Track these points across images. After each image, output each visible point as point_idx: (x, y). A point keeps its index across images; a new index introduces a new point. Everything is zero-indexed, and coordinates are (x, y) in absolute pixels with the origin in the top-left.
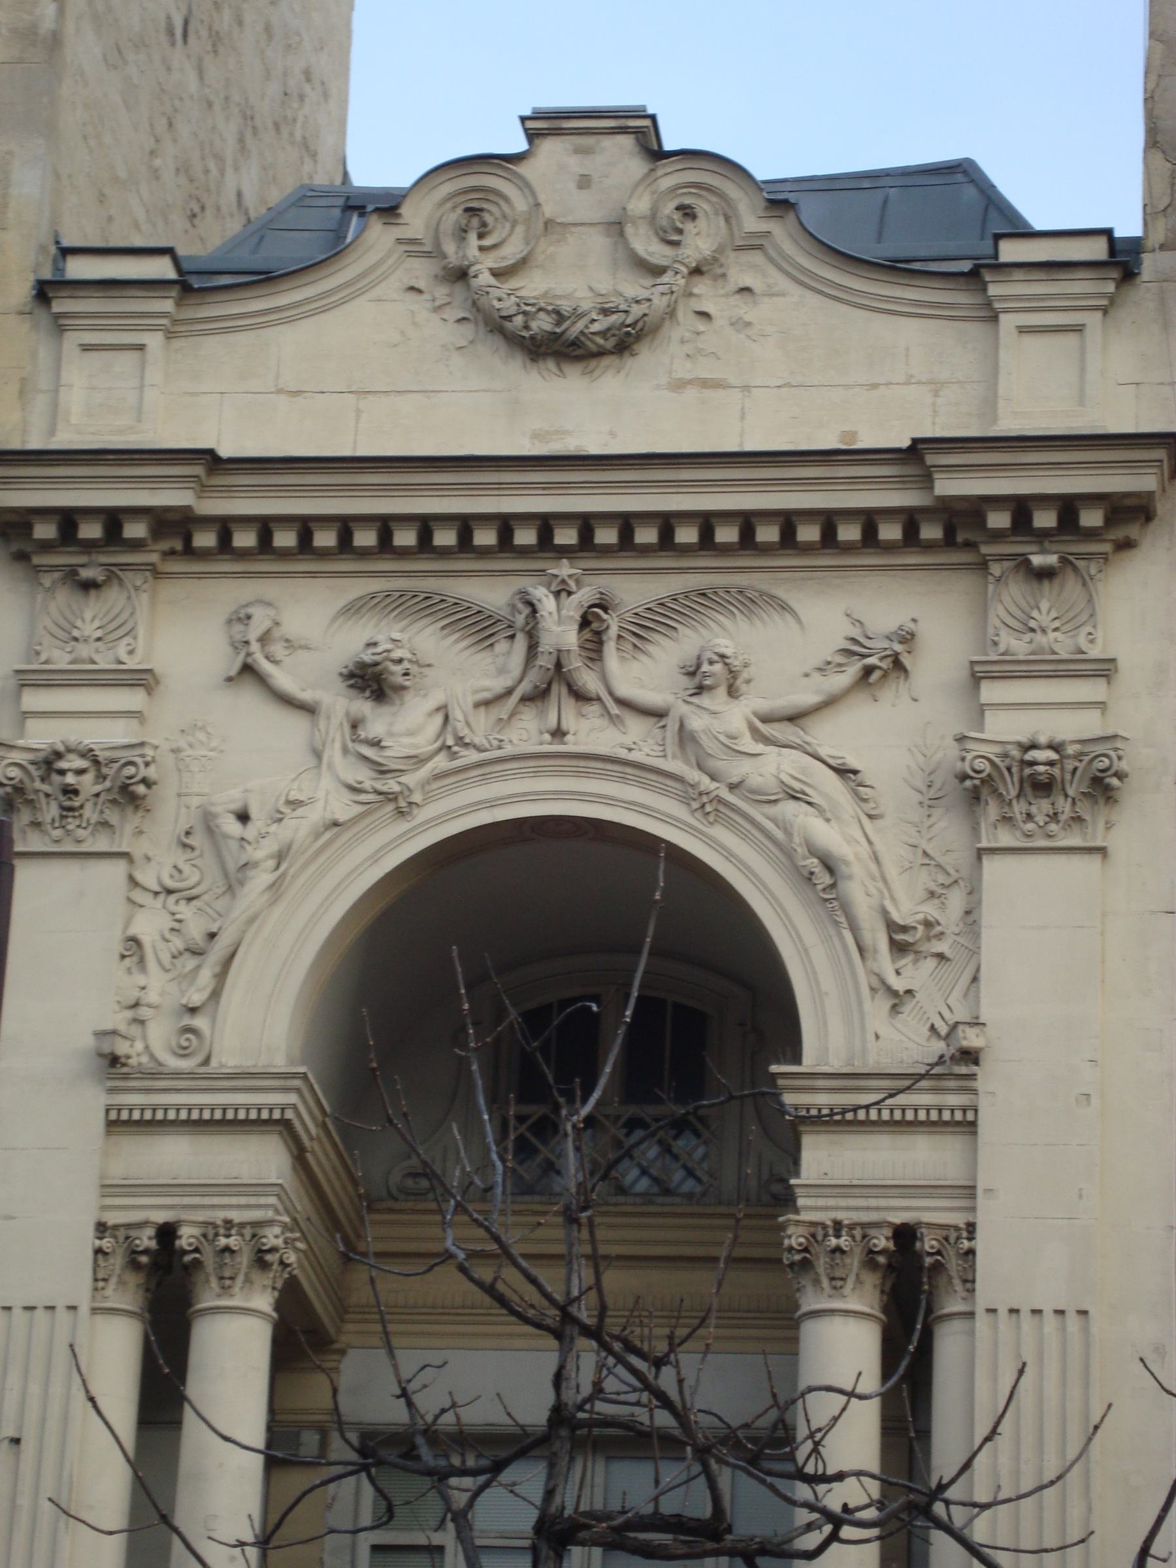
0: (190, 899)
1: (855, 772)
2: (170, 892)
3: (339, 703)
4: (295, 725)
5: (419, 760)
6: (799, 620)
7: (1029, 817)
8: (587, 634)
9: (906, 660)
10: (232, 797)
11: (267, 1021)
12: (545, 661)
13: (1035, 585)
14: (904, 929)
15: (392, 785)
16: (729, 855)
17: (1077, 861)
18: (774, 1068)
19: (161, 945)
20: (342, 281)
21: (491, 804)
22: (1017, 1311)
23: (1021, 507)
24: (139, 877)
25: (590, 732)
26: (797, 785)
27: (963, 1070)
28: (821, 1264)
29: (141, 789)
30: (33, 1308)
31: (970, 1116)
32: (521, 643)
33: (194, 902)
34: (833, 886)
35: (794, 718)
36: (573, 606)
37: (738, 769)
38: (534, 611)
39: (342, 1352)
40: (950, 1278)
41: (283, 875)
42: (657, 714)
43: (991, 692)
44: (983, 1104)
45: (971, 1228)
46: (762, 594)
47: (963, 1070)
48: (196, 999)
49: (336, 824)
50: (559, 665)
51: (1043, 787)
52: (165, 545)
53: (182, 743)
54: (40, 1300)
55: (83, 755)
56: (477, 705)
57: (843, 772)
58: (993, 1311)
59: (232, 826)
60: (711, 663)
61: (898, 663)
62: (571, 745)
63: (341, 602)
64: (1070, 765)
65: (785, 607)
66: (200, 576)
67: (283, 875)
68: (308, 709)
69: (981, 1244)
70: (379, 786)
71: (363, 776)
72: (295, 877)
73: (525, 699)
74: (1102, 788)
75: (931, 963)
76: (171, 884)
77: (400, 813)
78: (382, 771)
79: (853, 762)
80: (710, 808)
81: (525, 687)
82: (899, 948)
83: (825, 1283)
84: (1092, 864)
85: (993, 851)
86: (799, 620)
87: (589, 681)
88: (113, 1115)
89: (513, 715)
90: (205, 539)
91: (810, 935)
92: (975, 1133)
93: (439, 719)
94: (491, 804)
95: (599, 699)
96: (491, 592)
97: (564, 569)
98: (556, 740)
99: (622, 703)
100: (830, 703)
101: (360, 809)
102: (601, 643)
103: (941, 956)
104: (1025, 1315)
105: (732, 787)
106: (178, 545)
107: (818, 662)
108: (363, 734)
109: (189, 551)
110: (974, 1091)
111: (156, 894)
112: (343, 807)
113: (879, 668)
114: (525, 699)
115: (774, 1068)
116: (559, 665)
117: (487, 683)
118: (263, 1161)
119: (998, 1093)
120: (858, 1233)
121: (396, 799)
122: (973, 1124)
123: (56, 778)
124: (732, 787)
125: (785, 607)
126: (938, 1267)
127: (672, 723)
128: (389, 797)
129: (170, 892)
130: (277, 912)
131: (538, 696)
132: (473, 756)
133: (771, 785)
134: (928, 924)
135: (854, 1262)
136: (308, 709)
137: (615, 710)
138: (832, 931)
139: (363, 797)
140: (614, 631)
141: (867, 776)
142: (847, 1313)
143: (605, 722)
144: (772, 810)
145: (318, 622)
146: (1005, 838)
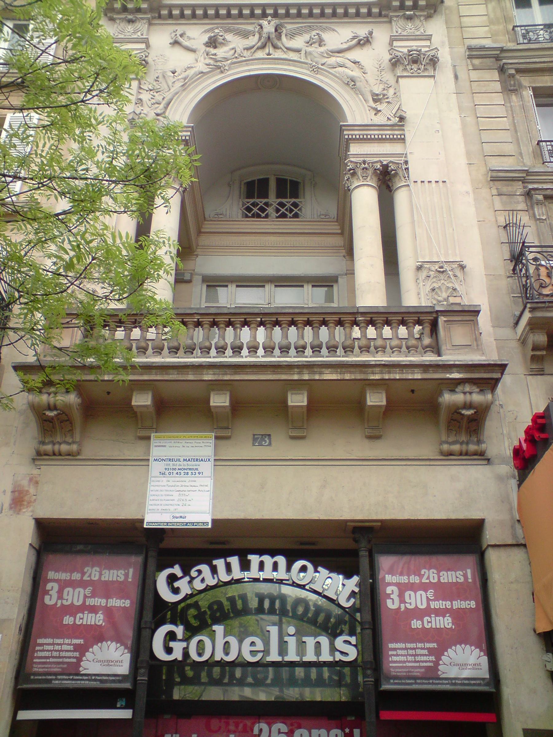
1: (358, 62)
2: (151, 90)
5: (226, 59)
6: (338, 33)
7: (412, 69)
8: (277, 33)
9: (370, 39)
10: (172, 68)
13: (406, 20)
14: (377, 95)
15: (219, 64)
16: (322, 81)
17: (427, 79)
19: (148, 101)
21: (249, 71)
22: (423, 182)
24: (142, 86)
28: (359, 172)
31: (403, 137)
33: (158, 93)
38: (262, 27)
39: (197, 255)
40: (400, 177)
41: (186, 83)
43: (395, 44)
44: (407, 133)
45: (406, 162)
48: (159, 111)
49: (202, 73)
50: (269, 38)
51: (415, 61)
53: (156, 58)
56: (244, 49)
58: (415, 182)
60: (314, 36)
65: (334, 30)
66: (162, 24)
67: (186, 83)
69: (410, 166)
70: (215, 64)
72: (190, 85)
73: (258, 48)
76: (151, 88)
77: (222, 72)
78: (217, 61)
80: (316, 70)
81: (259, 44)
82: (375, 101)
83: (361, 178)
84: (431, 80)
85: (402, 77)
86: (338, 33)
92: (404, 143)
93: (233, 51)
94: (249, 71)
95: (281, 48)
98: (221, 354)
102: (281, 36)
103: (388, 102)
104: (426, 183)
109: (160, 17)
110: (404, 130)
111: (147, 91)
112: (206, 69)
114: (258, 48)
116: (269, 38)
119: (409, 133)
120: (370, 165)
121: (220, 68)
122: (404, 139)
124: (322, 65)
125: (334, 30)
126: (396, 174)
127: (303, 52)
128: (219, 67)
129: (151, 90)
130: (184, 93)
131: (263, 47)
133: (335, 64)
134: (384, 95)
135: (370, 172)
136: (193, 51)
137: (285, 50)
138: (355, 96)
139: (211, 67)
140: (284, 32)
141: (363, 63)
142: (369, 185)
143: (283, 53)
144: (335, 70)
146: (405, 74)
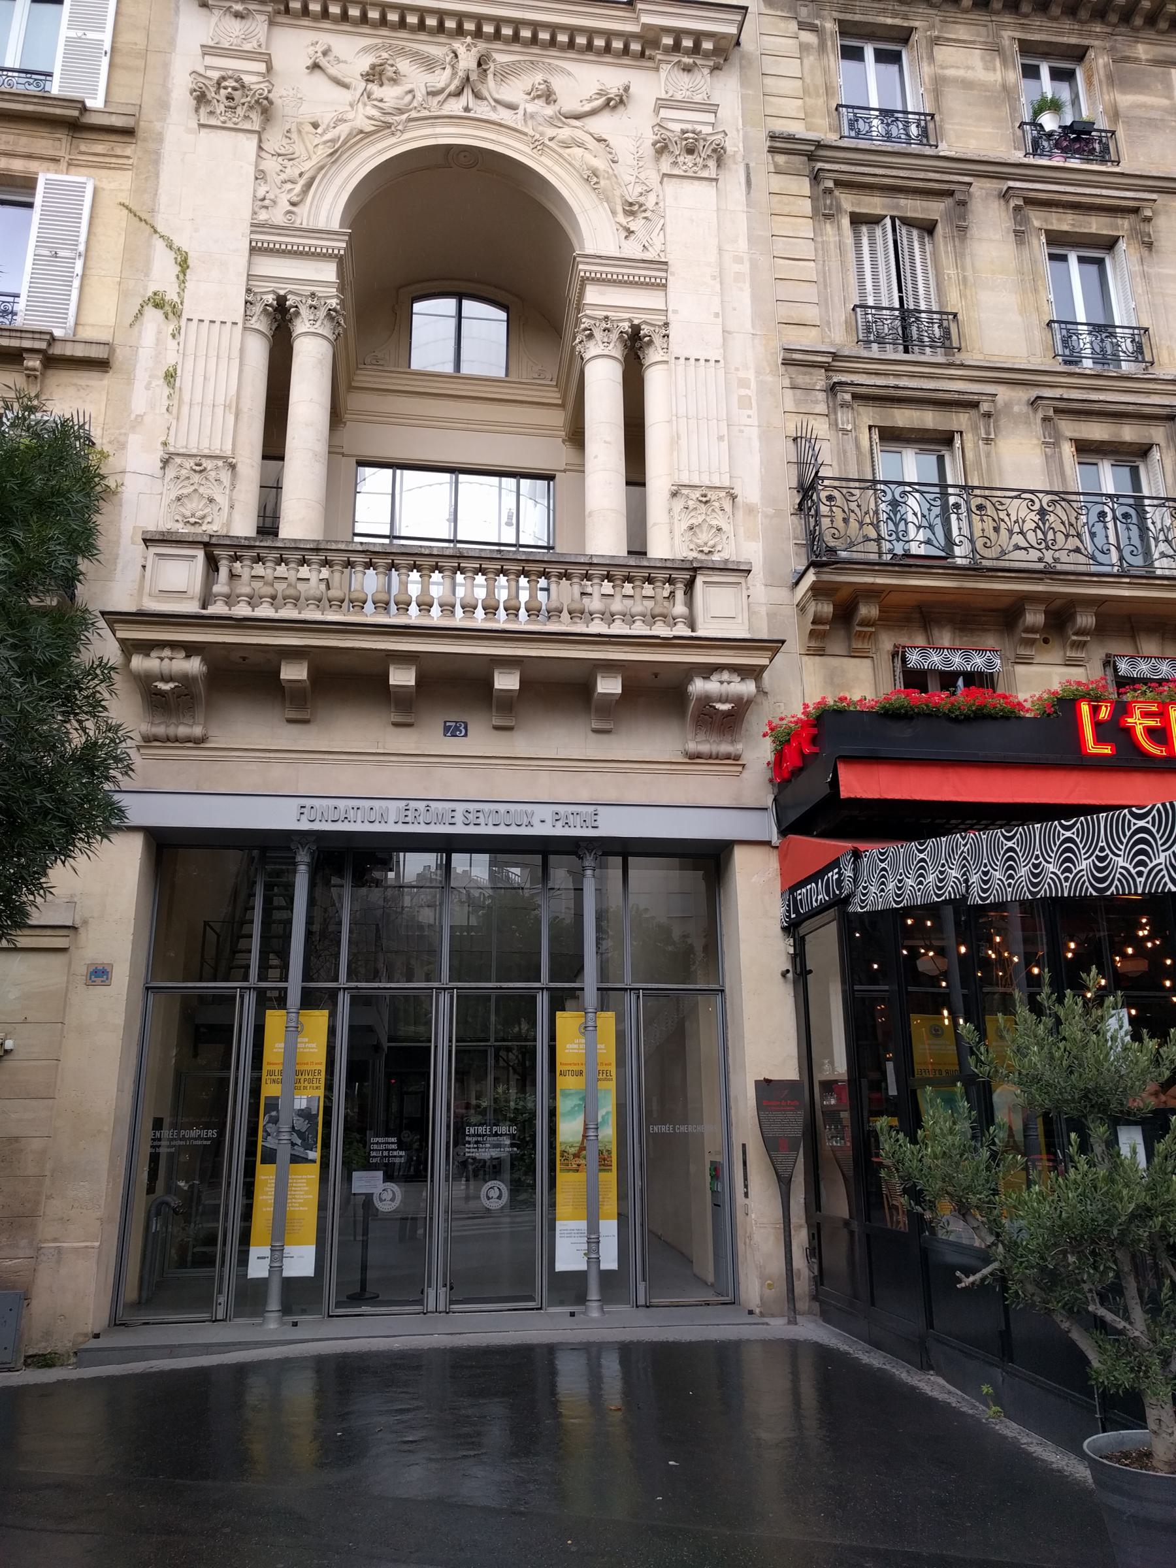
2: (279, 155)
11: (328, 209)
12: (461, 74)
20: (418, 286)
23: (678, 34)
25: (482, 110)
30: (407, 1219)
31: (664, 281)
32: (448, 71)
35: (578, 117)
50: (468, 79)
54: (218, 319)
55: (236, 81)
57: (600, 140)
61: (621, 101)
64: (702, 143)
71: (375, 113)
74: (749, 571)
79: (604, 137)
81: (452, 88)
88: (254, 244)
95: (486, 99)
96: (436, 49)
99: (496, 101)
101: (374, 128)
106: (282, 8)
108: (373, 97)
113: (615, 103)
114: (450, 95)
118: (328, 272)
122: (665, 286)
123: (222, 91)
127: (521, 111)
129: (279, 155)
137: (493, 103)
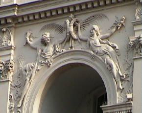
0: (117, 18)
3: (39, 47)
4: (32, 52)
6: (108, 19)
8: (75, 28)
16: (97, 66)
18: (101, 107)
26: (106, 51)
27: (129, 102)
29: (10, 68)
34: (111, 70)
36: (73, 22)
37: (98, 49)
42: (86, 41)
46: (102, 15)
47: (129, 102)
52: (15, 22)
59: (24, 73)
62: (73, 49)
63: (41, 28)
65: (106, 17)
68: (35, 49)
75: (127, 82)
86: (108, 19)
87: (75, 36)
89: (65, 45)
90: (20, 20)
91: (107, 77)
97: (72, 16)
99: (81, 40)
100: (112, 35)
103: (128, 81)
105: (97, 53)
107: (111, 26)
114: (66, 42)
115: (101, 107)
117: (61, 39)
132: (58, 54)
136: (35, 49)
140: (79, 26)
145: (34, 34)
